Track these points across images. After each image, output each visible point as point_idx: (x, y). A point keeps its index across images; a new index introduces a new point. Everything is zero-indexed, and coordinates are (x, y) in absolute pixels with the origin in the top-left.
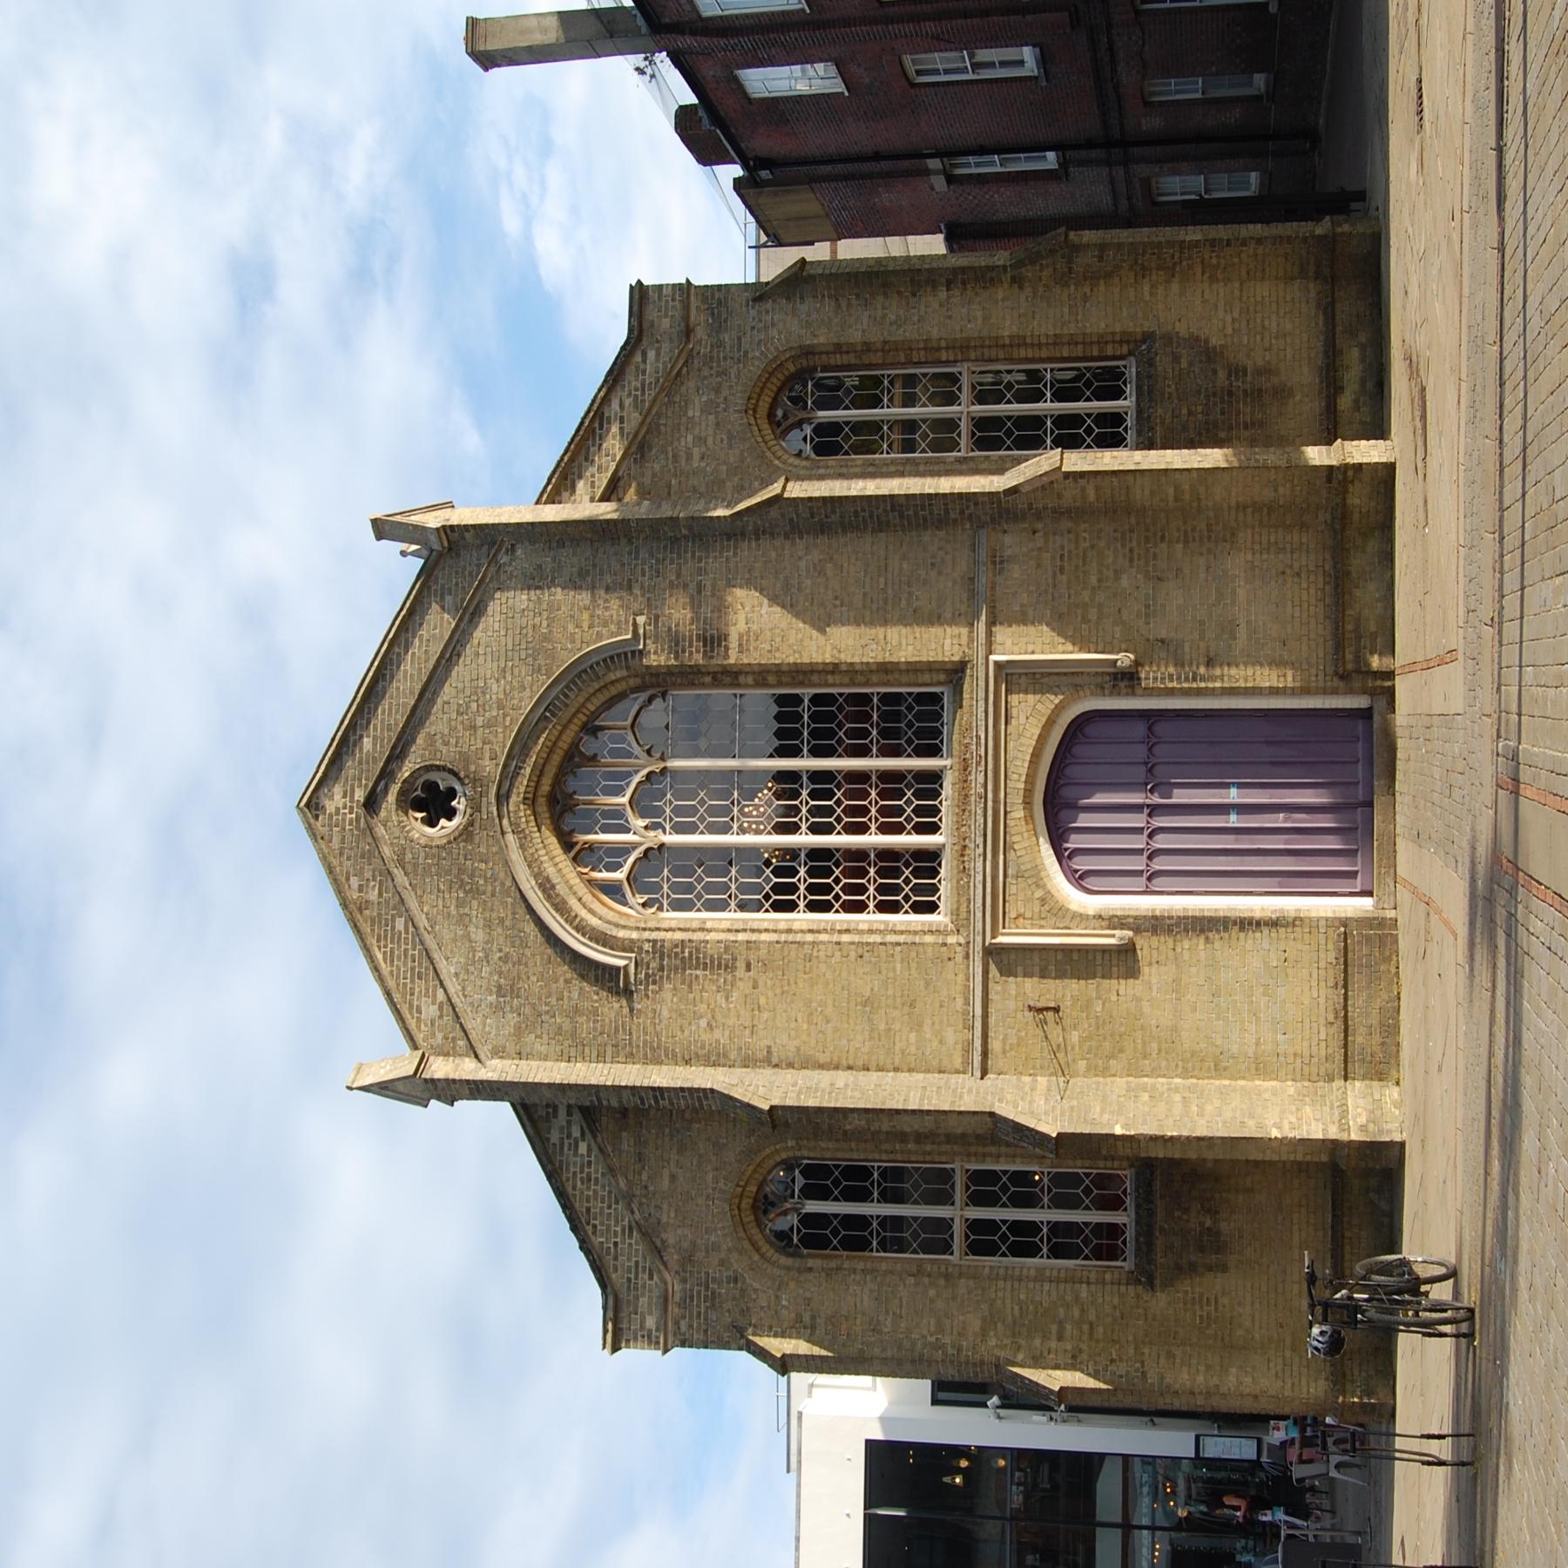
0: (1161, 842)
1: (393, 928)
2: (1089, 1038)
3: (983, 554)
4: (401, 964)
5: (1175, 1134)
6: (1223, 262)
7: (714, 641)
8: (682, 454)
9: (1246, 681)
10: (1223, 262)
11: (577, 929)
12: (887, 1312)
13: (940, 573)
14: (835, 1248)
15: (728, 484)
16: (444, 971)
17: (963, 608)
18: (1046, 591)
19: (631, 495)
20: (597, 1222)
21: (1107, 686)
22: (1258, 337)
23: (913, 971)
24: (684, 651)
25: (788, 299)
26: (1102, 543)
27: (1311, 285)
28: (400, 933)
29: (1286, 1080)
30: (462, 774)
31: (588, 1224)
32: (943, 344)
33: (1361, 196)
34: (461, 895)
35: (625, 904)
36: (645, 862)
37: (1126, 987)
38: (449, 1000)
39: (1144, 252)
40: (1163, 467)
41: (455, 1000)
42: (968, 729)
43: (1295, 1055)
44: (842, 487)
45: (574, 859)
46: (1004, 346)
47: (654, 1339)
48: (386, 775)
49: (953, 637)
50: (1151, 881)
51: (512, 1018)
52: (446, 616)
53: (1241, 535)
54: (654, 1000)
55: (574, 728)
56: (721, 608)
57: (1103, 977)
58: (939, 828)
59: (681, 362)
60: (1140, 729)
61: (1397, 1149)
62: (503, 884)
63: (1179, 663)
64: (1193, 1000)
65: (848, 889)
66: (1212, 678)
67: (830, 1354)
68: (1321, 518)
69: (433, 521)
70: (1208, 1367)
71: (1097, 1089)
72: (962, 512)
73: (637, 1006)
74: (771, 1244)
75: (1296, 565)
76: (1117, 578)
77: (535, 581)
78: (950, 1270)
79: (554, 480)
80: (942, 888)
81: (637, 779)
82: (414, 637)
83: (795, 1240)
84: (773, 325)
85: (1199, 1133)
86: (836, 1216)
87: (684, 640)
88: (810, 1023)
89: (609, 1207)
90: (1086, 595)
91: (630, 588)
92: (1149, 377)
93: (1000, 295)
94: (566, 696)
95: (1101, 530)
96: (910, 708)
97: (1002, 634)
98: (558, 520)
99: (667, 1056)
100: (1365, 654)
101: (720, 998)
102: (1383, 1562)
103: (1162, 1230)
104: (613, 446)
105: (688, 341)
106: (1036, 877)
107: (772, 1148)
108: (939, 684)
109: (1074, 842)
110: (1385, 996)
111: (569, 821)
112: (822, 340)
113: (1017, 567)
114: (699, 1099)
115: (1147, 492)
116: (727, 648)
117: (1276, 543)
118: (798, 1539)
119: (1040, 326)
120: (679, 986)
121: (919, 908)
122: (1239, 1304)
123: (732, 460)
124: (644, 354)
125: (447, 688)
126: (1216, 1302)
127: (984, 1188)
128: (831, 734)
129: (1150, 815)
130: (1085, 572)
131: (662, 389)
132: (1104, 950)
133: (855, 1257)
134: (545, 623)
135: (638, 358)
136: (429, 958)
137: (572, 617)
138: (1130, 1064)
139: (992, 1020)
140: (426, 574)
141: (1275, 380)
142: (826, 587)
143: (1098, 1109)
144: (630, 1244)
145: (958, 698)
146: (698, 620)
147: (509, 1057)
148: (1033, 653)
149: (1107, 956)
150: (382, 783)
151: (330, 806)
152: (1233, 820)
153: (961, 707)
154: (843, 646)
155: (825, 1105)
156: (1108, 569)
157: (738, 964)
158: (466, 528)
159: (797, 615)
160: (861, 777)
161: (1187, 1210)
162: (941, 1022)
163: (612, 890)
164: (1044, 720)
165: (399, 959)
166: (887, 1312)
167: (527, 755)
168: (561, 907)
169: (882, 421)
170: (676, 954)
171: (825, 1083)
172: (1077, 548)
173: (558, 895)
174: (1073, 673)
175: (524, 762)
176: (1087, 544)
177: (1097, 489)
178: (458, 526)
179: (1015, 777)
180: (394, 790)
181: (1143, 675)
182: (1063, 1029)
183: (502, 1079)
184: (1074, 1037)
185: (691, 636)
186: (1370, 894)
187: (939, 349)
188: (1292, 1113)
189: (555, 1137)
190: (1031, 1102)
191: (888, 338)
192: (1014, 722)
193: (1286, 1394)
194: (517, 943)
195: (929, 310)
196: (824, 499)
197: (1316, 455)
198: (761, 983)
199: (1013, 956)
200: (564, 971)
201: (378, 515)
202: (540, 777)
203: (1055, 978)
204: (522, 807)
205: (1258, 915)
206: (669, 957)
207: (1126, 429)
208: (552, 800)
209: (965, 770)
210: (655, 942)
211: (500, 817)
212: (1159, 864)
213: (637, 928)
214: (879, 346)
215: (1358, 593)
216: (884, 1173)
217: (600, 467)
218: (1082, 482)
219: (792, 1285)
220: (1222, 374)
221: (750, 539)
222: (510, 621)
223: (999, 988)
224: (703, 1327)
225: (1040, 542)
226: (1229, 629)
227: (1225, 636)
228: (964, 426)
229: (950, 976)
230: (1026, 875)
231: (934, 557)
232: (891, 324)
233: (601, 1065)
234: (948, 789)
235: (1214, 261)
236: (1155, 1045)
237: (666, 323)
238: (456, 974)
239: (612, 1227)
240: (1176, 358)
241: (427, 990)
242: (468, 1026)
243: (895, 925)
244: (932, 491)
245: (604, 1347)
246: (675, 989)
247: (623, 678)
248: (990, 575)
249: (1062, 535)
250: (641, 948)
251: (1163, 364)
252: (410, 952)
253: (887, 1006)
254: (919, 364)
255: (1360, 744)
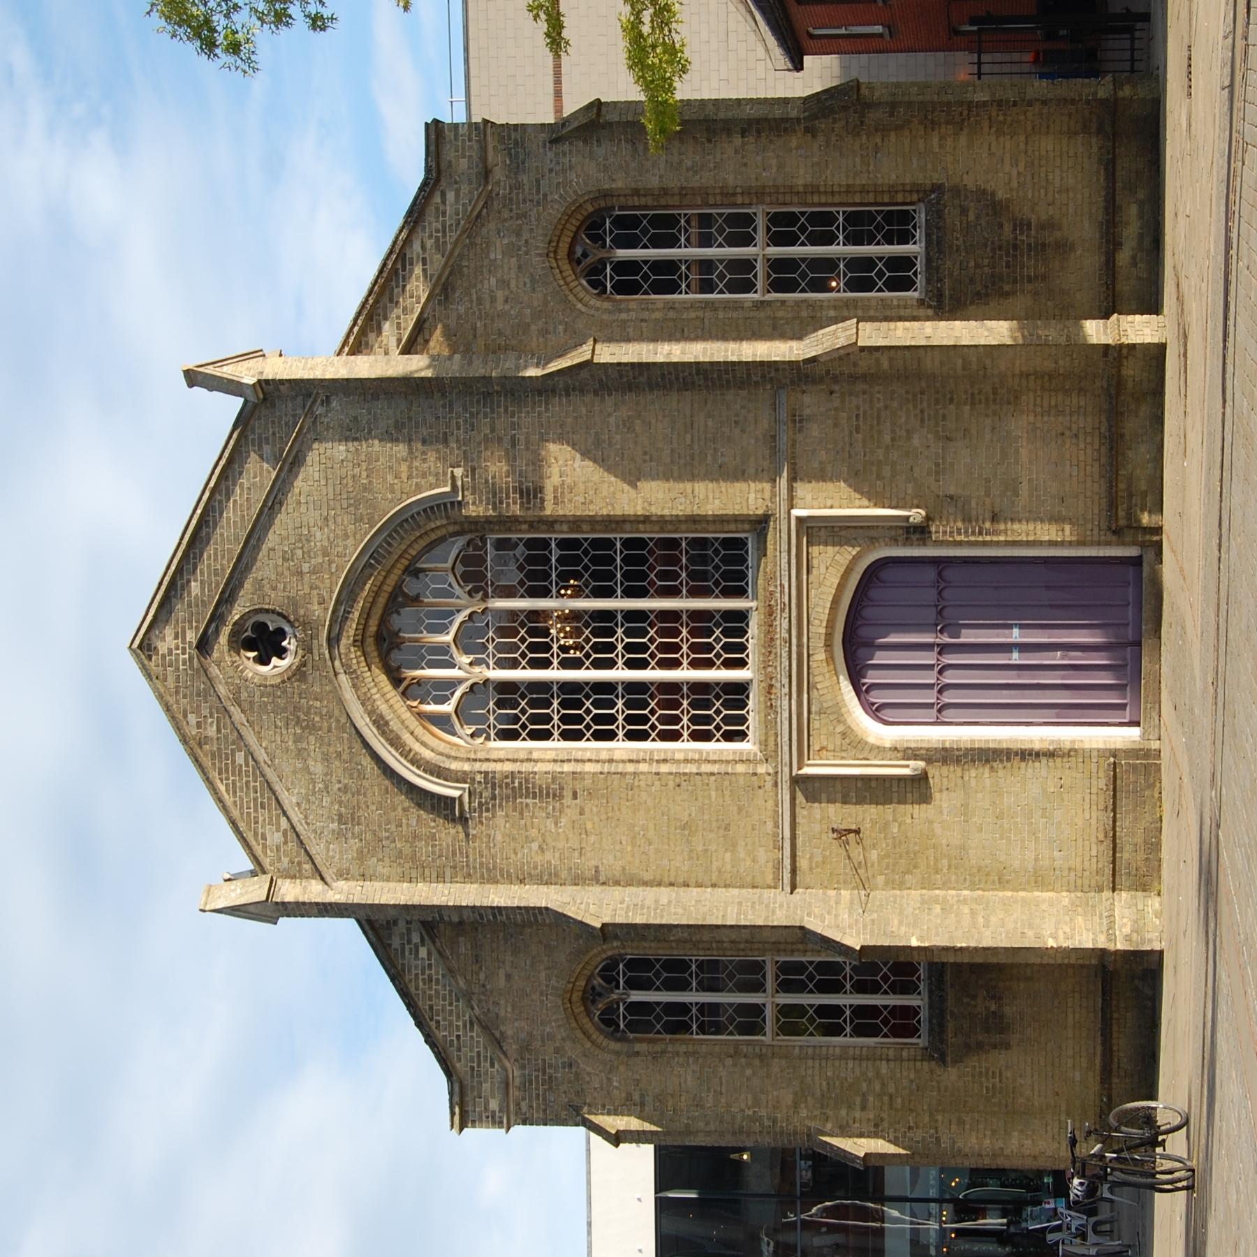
0: (950, 678)
1: (234, 762)
2: (887, 856)
3: (784, 415)
4: (243, 795)
5: (964, 945)
6: (1009, 119)
7: (531, 493)
8: (486, 296)
9: (1028, 535)
10: (1009, 119)
11: (412, 762)
12: (709, 1090)
13: (743, 431)
14: (659, 1032)
15: (533, 327)
16: (286, 802)
17: (766, 464)
18: (843, 450)
19: (437, 341)
20: (440, 1018)
21: (900, 539)
22: (1042, 191)
23: (727, 798)
24: (501, 503)
25: (585, 141)
26: (895, 404)
27: (1094, 140)
28: (241, 766)
29: (1062, 891)
30: (292, 618)
31: (431, 1019)
32: (739, 190)
33: (1146, 17)
34: (299, 731)
35: (454, 734)
36: (471, 696)
37: (920, 811)
38: (293, 827)
39: (934, 110)
40: (952, 343)
41: (299, 828)
42: (774, 578)
43: (1069, 869)
44: (648, 351)
45: (404, 694)
46: (798, 192)
47: (497, 1119)
48: (217, 618)
49: (756, 492)
50: (940, 713)
51: (355, 844)
52: (265, 465)
53: (1024, 397)
54: (488, 826)
55: (397, 572)
56: (538, 463)
57: (899, 803)
58: (747, 663)
59: (481, 203)
60: (930, 574)
61: (1157, 956)
62: (338, 721)
63: (967, 519)
64: (979, 822)
65: (664, 720)
66: (996, 533)
67: (659, 1129)
68: (1098, 384)
69: (247, 374)
70: (994, 1132)
71: (895, 902)
72: (763, 376)
73: (472, 832)
74: (601, 1031)
75: (1074, 427)
76: (909, 438)
77: (352, 432)
78: (764, 1050)
79: (360, 322)
80: (750, 718)
81: (460, 618)
82: (235, 485)
83: (622, 1026)
84: (571, 168)
85: (984, 944)
86: (658, 1004)
87: (501, 492)
88: (633, 845)
89: (451, 1004)
90: (880, 453)
91: (445, 442)
92: (939, 228)
93: (794, 143)
94: (389, 544)
95: (893, 392)
96: (716, 552)
97: (802, 489)
98: (373, 376)
99: (502, 876)
100: (1136, 511)
101: (550, 823)
102: (1134, 525)
103: (952, 1013)
104: (418, 289)
105: (487, 182)
106: (838, 714)
107: (600, 949)
108: (744, 531)
109: (871, 678)
110: (1148, 817)
111: (396, 657)
112: (620, 184)
113: (815, 426)
114: (535, 915)
115: (937, 363)
116: (543, 500)
117: (1056, 406)
118: (589, 1224)
119: (833, 175)
120: (510, 812)
121: (729, 737)
122: (1021, 1076)
123: (536, 303)
124: (443, 195)
125: (270, 535)
126: (1000, 1075)
127: (791, 977)
128: (643, 576)
129: (940, 653)
130: (879, 432)
131: (464, 232)
132: (900, 779)
133: (677, 1040)
134: (364, 474)
135: (437, 199)
136: (271, 789)
137: (391, 468)
138: (923, 878)
139: (799, 841)
140: (243, 421)
141: (1058, 234)
142: (636, 443)
143: (896, 922)
144: (472, 1037)
145: (762, 547)
146: (514, 472)
147: (354, 879)
148: (832, 507)
149: (902, 784)
150: (213, 625)
151: (163, 648)
152: (1016, 658)
153: (765, 555)
154: (653, 499)
155: (652, 921)
156: (901, 429)
157: (565, 793)
158: (282, 382)
159: (609, 470)
160: (673, 615)
161: (974, 997)
162: (754, 843)
163: (441, 721)
164: (842, 570)
165: (241, 791)
166: (709, 1090)
167: (355, 601)
168: (395, 742)
169: (680, 261)
170: (507, 784)
171: (649, 901)
172: (872, 408)
173: (392, 731)
174: (868, 527)
175: (352, 607)
176: (881, 404)
177: (891, 360)
178: (273, 380)
179: (817, 622)
180: (226, 632)
181: (933, 529)
182: (864, 848)
183: (350, 902)
184: (874, 855)
185: (508, 488)
186: (1137, 724)
187: (734, 194)
188: (1066, 923)
189: (396, 942)
190: (836, 916)
191: (685, 184)
192: (815, 572)
193: (1061, 1154)
194: (355, 775)
195: (725, 156)
196: (632, 364)
197: (1095, 331)
198: (587, 810)
199: (817, 785)
200: (402, 800)
201: (191, 367)
202: (367, 619)
203: (856, 804)
204: (352, 649)
205: (1037, 746)
206: (500, 787)
207: (915, 274)
208: (379, 638)
209: (771, 615)
210: (486, 773)
211: (332, 659)
212: (948, 698)
213: (468, 759)
214: (676, 190)
215: (1130, 454)
216: (701, 965)
217: (405, 309)
218: (877, 354)
219: (622, 1068)
220: (1007, 228)
221: (560, 395)
222: (329, 471)
223: (805, 813)
224: (542, 1107)
225: (837, 403)
226: (1012, 487)
227: (1009, 494)
228: (760, 268)
229: (761, 802)
230: (828, 712)
231: (737, 415)
232: (687, 170)
233: (441, 885)
234: (754, 628)
235: (1001, 118)
236: (945, 862)
237: (464, 163)
238: (298, 804)
239: (454, 1023)
240: (964, 211)
241: (271, 819)
242: (313, 852)
243: (708, 753)
244: (735, 359)
245: (452, 1126)
246: (507, 816)
247: (443, 526)
248: (791, 432)
249: (858, 396)
250: (473, 780)
251: (951, 215)
252: (252, 784)
253: (704, 829)
254: (715, 205)
255: (1131, 589)
